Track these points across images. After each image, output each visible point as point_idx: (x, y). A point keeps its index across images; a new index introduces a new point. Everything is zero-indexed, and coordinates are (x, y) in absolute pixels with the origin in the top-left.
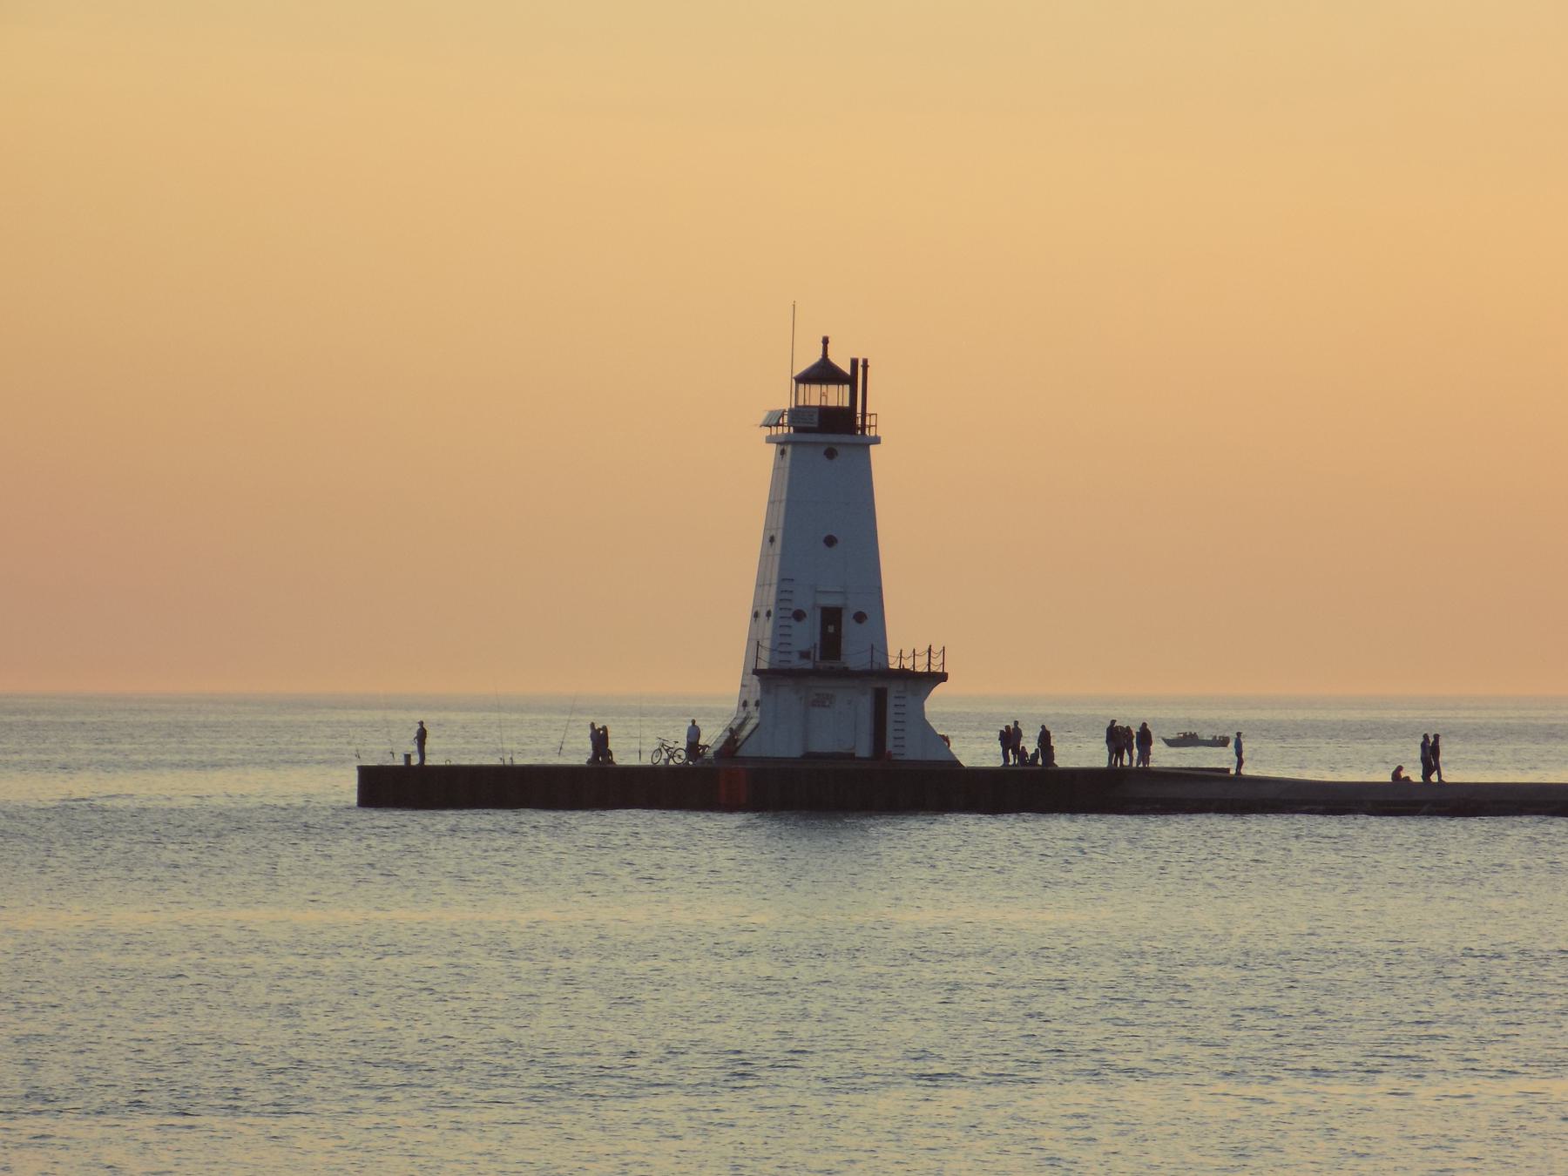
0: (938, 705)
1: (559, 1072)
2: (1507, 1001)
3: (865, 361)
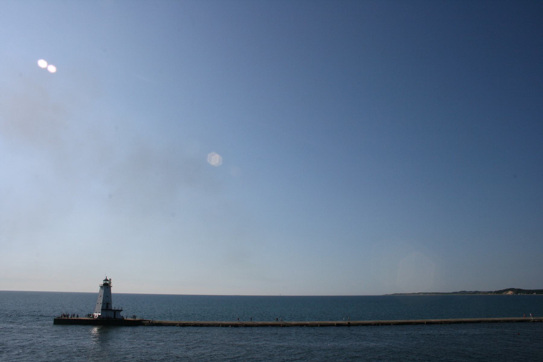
0: (122, 314)
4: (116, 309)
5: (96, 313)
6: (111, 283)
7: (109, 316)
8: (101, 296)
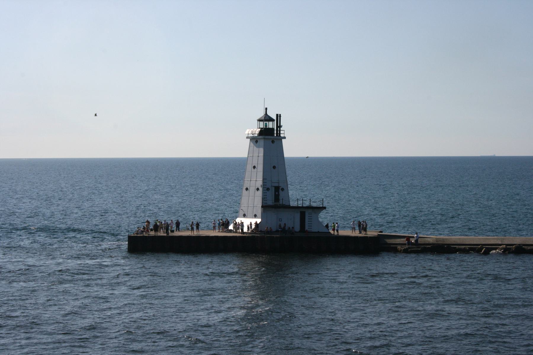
0: (324, 218)
1: (336, 300)
2: (5, 235)
3: (280, 115)
4: (307, 204)
5: (244, 216)
6: (280, 127)
7: (287, 228)
8: (254, 167)
